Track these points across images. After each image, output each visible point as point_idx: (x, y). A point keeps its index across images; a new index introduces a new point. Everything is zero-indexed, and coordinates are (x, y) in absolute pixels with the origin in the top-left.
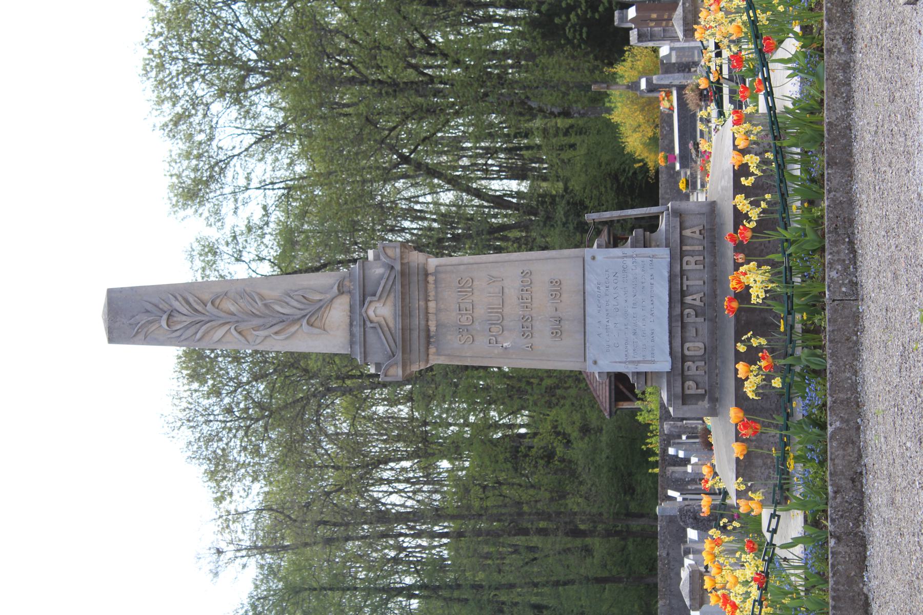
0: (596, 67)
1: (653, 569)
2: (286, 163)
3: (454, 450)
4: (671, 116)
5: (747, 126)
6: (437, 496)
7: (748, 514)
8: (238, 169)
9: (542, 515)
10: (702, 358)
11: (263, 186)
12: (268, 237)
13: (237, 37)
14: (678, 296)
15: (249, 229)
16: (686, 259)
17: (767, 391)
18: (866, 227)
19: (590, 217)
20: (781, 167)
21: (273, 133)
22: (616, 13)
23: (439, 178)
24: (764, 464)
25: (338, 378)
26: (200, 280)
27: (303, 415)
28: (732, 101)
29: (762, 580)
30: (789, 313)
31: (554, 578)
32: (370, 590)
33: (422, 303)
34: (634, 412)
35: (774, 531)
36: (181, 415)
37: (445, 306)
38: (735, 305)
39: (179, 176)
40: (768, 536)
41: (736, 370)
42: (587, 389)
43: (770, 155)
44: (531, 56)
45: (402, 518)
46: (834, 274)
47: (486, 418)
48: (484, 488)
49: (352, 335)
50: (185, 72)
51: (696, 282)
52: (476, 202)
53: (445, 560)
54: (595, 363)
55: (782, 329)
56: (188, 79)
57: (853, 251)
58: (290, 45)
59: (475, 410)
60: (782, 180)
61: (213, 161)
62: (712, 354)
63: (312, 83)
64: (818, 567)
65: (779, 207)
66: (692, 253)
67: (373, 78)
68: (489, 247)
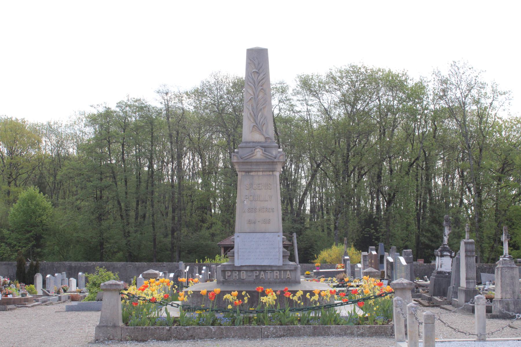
0: (353, 240)
1: (159, 261)
2: (317, 119)
3: (206, 184)
4: (334, 268)
5: (330, 295)
6: (187, 178)
7: (179, 296)
8: (315, 101)
9: (180, 218)
10: (240, 278)
11: (308, 111)
12: (289, 113)
13: (365, 101)
14: (264, 269)
15: (292, 105)
16: (278, 272)
17: (226, 303)
18: (290, 341)
19: (295, 235)
20: (313, 309)
21: (329, 115)
22: (374, 247)
23: (311, 179)
24: (198, 302)
25: (234, 139)
26: (271, 87)
27: (220, 126)
28: (339, 291)
29: (153, 301)
30: (257, 312)
31: (155, 223)
32: (151, 152)
33: (261, 170)
34: (220, 254)
35: (172, 305)
36: (220, 79)
37: (260, 178)
38: (260, 291)
39: (312, 79)
40: (171, 303)
41: (235, 291)
42: (229, 236)
43: (318, 304)
44: (358, 214)
45: (179, 164)
46: (272, 329)
47: (218, 197)
48: (191, 196)
49: (249, 142)
50: (352, 81)
51: (269, 276)
52: (302, 194)
53: (163, 181)
54: (238, 237)
55: (251, 309)
56: (349, 82)
57: (281, 336)
58: (363, 122)
59: (221, 192)
60: (308, 309)
61: (318, 92)
62: (242, 282)
63: (348, 130)
64: (158, 322)
65: (298, 308)
66: (280, 274)
67: (350, 154)
68: (284, 198)
